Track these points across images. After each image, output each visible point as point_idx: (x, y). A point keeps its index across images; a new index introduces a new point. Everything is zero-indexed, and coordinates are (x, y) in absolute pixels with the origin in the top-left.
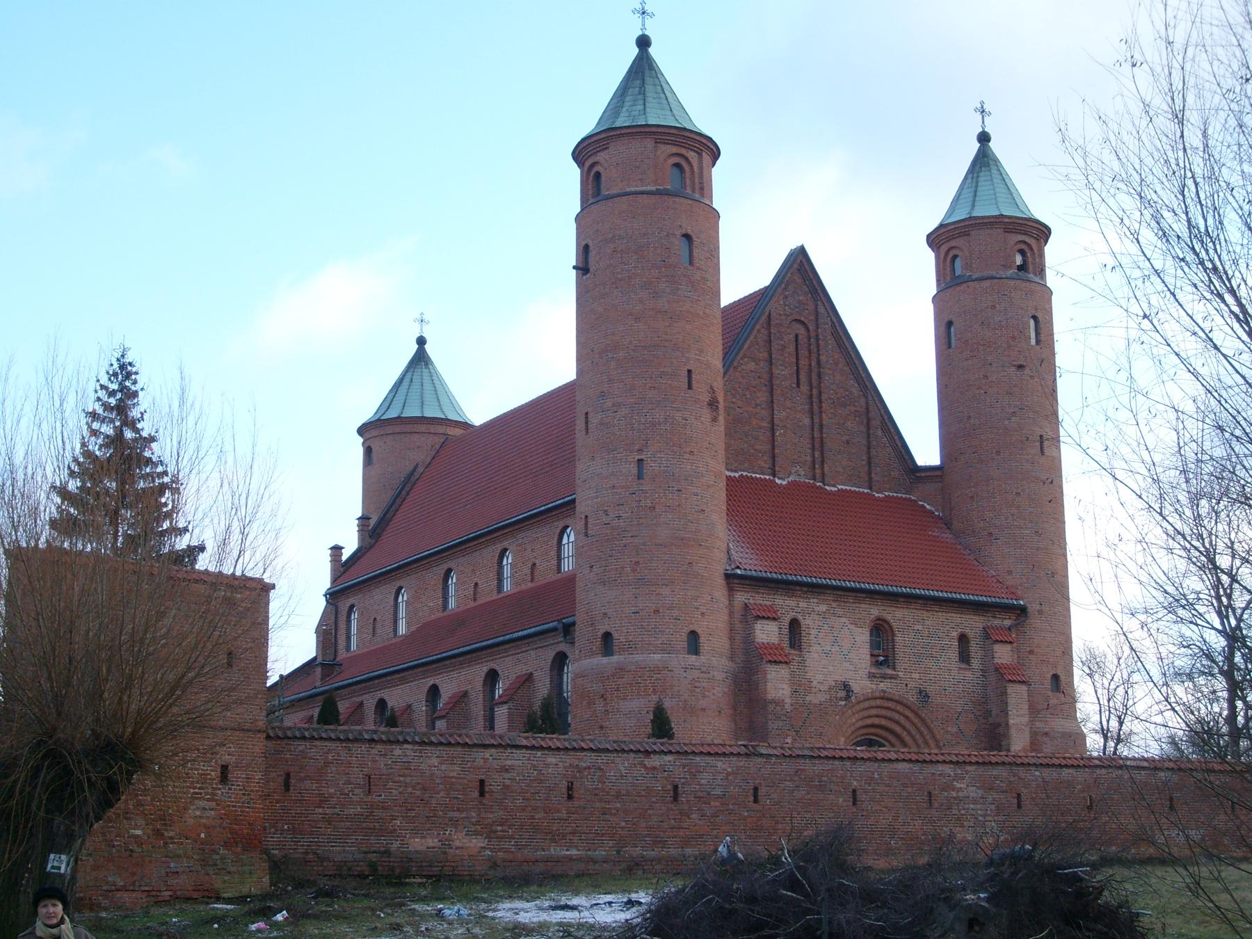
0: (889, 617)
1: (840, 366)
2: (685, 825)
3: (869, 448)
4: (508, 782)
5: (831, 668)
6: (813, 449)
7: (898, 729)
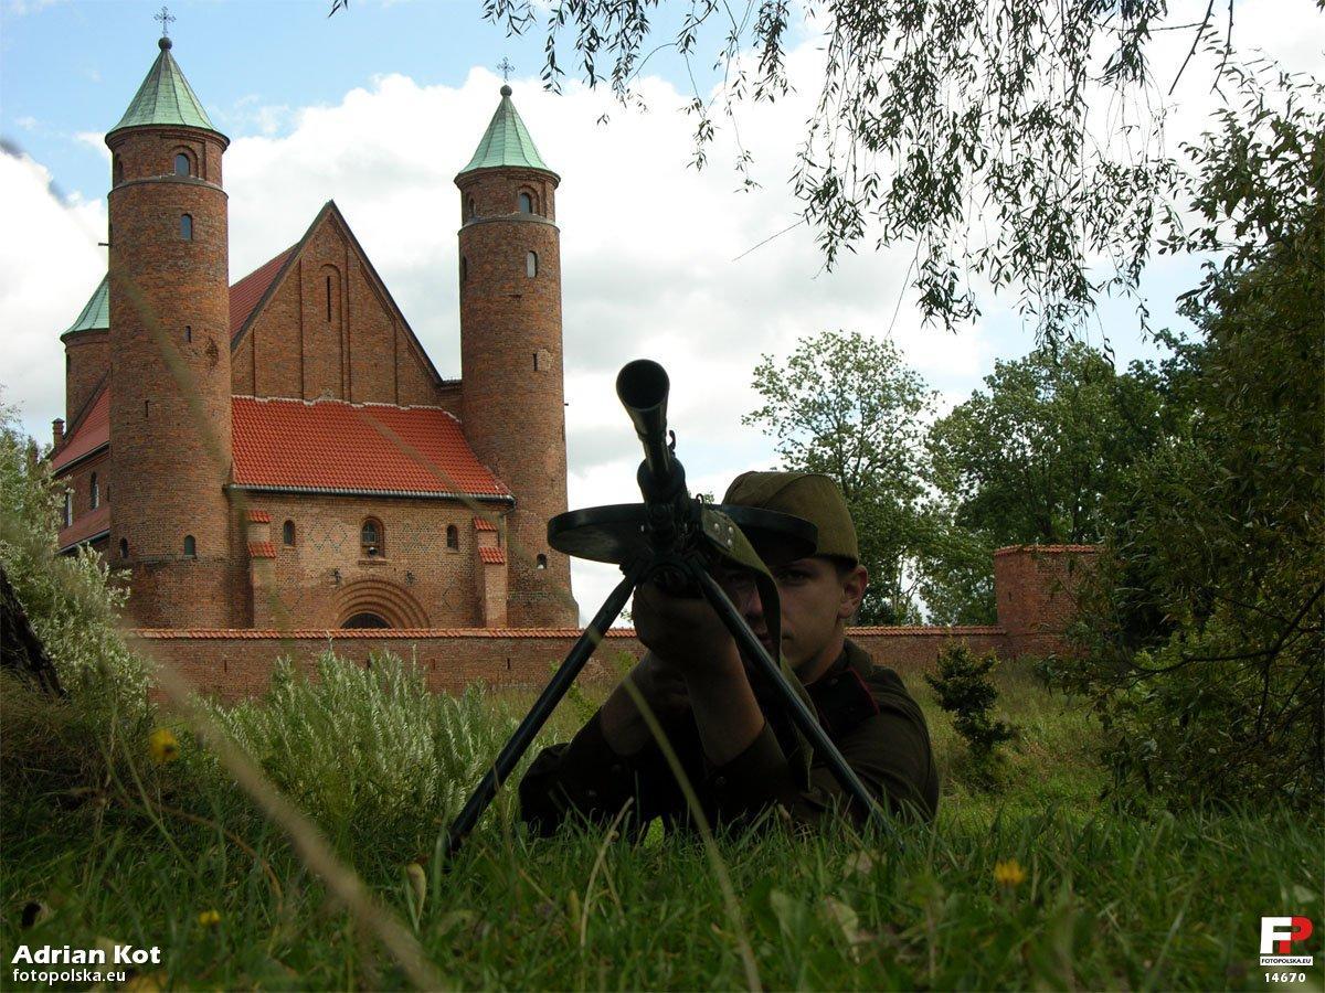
0: (379, 515)
1: (370, 300)
6: (342, 373)
7: (390, 605)
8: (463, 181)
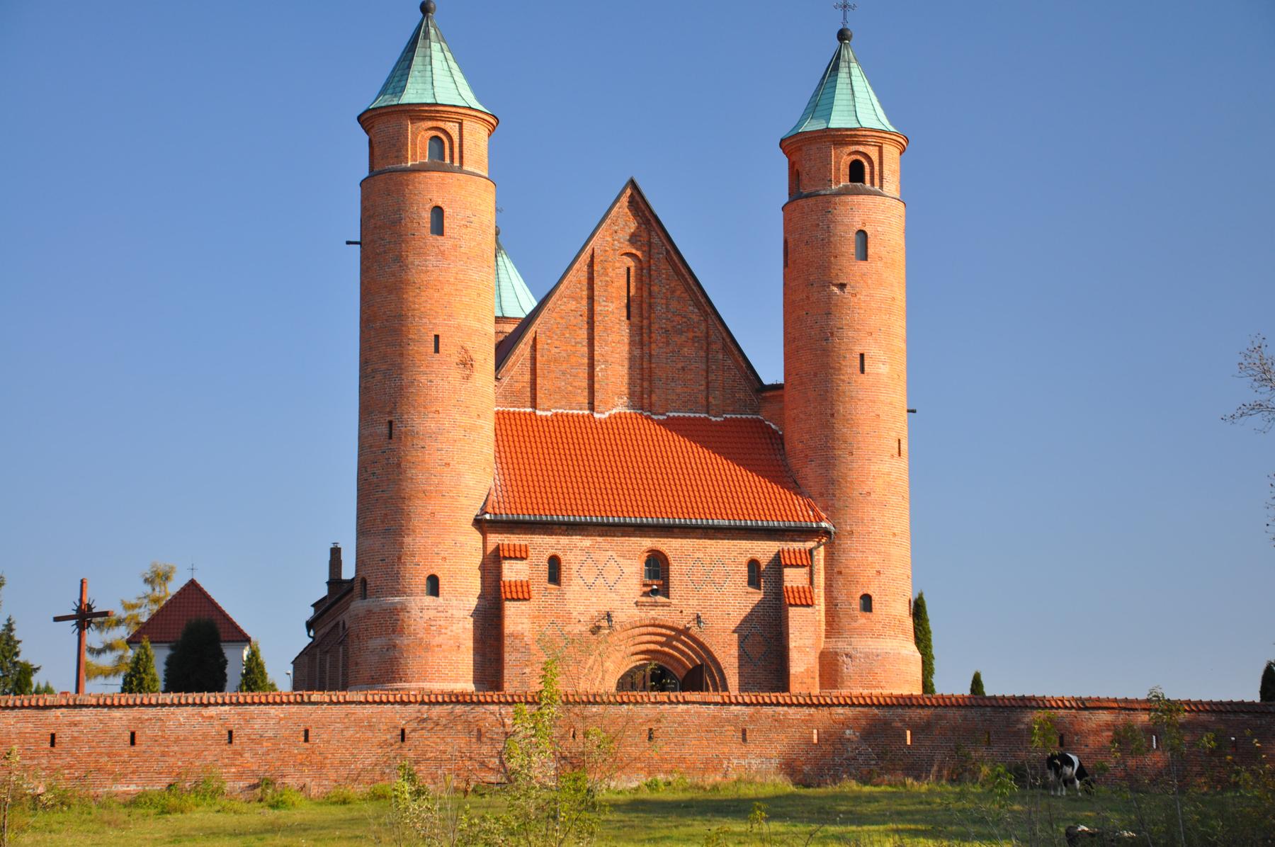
1: (678, 293)
2: (237, 762)
3: (707, 372)
4: (76, 734)
5: (594, 600)
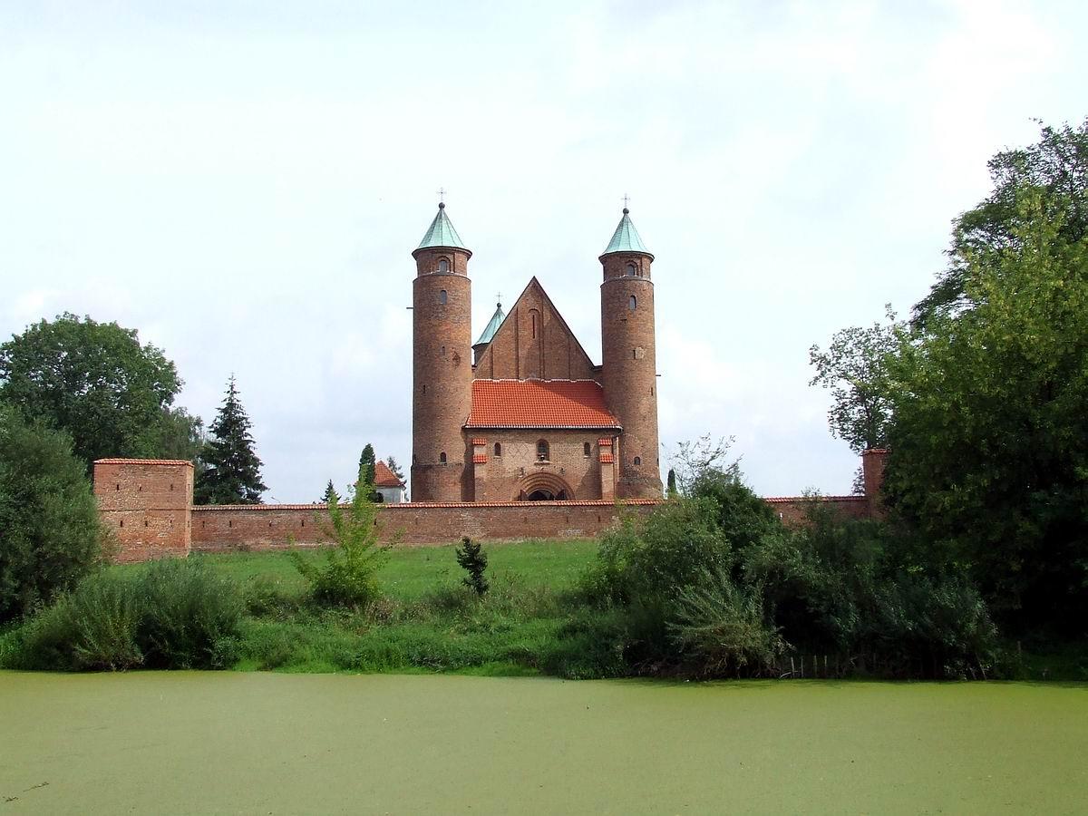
8: (604, 259)
